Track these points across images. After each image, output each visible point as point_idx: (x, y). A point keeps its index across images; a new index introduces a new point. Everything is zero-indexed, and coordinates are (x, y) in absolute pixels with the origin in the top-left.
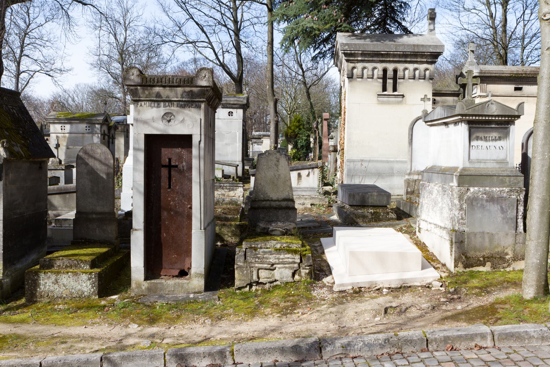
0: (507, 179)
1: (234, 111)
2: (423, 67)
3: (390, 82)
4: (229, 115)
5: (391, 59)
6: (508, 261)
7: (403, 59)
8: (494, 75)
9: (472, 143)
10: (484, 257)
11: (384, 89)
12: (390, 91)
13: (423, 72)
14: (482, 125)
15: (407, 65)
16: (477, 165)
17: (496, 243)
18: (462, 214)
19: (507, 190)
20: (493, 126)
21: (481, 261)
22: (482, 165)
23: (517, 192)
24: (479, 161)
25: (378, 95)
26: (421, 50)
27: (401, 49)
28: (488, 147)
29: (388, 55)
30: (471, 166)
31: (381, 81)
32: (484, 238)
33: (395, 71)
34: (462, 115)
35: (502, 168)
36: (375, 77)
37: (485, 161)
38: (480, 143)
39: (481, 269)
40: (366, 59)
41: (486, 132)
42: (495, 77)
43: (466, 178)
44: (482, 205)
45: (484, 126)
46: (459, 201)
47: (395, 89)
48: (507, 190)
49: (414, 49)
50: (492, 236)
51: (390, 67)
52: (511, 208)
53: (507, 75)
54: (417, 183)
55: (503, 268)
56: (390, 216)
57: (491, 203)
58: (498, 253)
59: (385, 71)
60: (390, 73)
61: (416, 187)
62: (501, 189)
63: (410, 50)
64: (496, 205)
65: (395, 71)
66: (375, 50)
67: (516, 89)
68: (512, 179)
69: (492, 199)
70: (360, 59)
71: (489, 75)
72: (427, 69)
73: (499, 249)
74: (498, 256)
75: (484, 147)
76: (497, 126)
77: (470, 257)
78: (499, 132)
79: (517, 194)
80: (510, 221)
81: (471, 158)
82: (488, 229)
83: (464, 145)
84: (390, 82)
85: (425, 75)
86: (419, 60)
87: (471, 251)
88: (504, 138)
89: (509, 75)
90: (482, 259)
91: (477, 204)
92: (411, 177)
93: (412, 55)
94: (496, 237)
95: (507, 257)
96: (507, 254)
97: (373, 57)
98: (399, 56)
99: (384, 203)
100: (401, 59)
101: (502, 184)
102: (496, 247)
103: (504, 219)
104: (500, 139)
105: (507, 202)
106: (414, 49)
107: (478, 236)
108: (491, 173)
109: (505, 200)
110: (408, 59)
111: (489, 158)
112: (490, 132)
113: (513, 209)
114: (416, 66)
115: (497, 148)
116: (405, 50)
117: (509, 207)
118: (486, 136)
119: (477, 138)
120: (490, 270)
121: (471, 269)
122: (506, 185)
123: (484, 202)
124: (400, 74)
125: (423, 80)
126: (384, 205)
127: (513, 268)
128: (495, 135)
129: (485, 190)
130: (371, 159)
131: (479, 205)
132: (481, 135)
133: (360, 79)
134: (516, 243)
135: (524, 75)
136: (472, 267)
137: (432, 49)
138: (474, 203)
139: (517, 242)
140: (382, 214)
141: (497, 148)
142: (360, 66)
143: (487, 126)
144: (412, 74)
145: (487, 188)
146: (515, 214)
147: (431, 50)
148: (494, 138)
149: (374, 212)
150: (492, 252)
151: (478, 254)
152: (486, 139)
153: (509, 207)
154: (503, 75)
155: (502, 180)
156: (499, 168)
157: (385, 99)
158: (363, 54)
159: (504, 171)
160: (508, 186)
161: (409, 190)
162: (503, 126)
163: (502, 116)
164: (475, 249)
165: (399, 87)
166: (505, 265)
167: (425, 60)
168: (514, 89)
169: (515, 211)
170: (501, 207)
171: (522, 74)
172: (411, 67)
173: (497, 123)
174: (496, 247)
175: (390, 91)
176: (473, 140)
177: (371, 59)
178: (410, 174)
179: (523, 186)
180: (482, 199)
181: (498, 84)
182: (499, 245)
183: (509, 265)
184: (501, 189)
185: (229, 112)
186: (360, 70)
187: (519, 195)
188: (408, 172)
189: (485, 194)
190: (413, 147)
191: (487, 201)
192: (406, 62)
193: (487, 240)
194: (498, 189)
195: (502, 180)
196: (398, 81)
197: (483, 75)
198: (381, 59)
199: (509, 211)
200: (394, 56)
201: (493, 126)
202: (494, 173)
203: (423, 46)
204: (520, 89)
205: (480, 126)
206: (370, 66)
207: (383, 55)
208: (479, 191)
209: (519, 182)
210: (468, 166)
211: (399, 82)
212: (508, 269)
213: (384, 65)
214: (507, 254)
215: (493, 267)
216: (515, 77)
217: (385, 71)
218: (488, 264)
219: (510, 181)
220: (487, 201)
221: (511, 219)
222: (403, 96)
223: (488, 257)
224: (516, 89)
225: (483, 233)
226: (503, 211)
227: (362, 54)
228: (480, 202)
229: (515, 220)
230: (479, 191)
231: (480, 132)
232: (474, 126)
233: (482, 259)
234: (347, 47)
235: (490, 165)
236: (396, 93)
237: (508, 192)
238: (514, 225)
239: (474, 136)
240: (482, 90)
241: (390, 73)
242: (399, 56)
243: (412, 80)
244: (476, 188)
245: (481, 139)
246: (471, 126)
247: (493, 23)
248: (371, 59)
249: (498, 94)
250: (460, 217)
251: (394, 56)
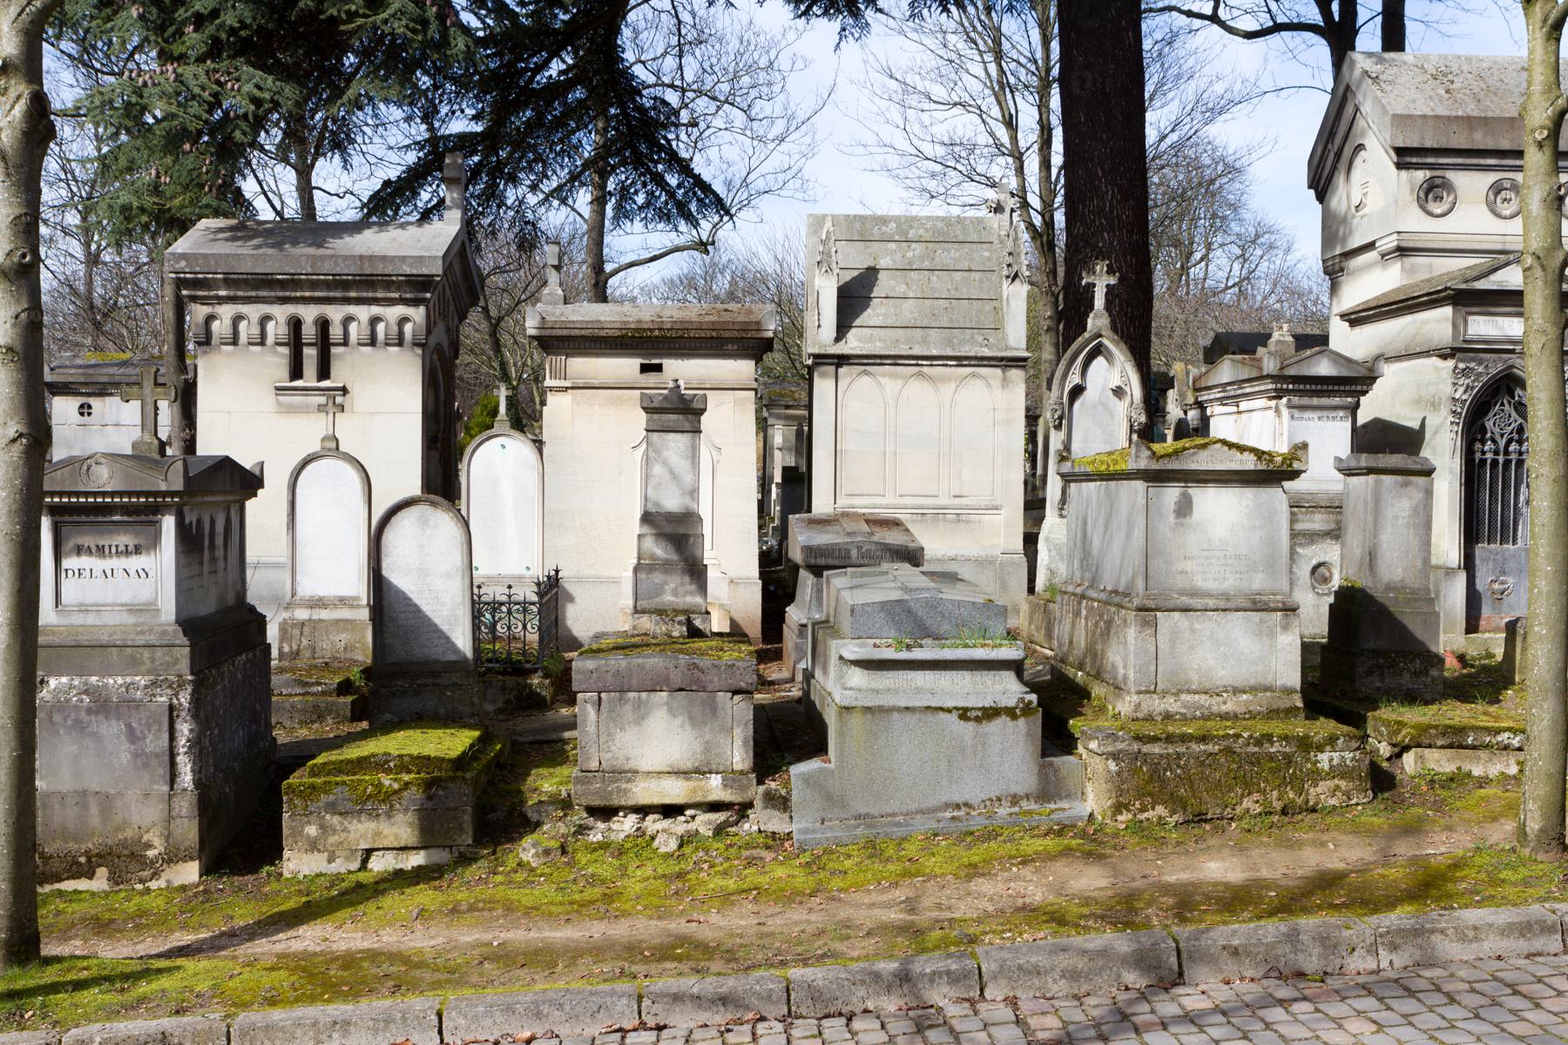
0: (146, 654)
1: (92, 401)
2: (394, 312)
3: (310, 353)
4: (82, 414)
5: (307, 294)
6: (152, 862)
7: (339, 295)
8: (577, 332)
9: (67, 563)
10: (87, 853)
11: (296, 372)
12: (310, 378)
13: (396, 328)
14: (87, 515)
15: (352, 309)
16: (77, 620)
17: (119, 819)
19: (142, 681)
20: (117, 518)
21: (81, 864)
22: (91, 619)
23: (170, 687)
24: (83, 608)
25: (277, 389)
26: (380, 269)
27: (327, 267)
28: (109, 573)
29: (293, 283)
30: (63, 621)
31: (285, 350)
32: (85, 807)
33: (323, 325)
35: (143, 624)
36: (270, 340)
37: (98, 608)
38: (85, 562)
39: (82, 884)
40: (241, 293)
41: (101, 533)
42: (583, 337)
44: (77, 722)
45: (92, 518)
47: (324, 372)
48: (142, 681)
49: (361, 267)
50: (107, 802)
51: (309, 314)
52: (155, 728)
53: (611, 333)
54: (306, 629)
55: (141, 881)
57: (101, 717)
58: (124, 844)
59: (296, 324)
60: (309, 331)
61: (305, 642)
62: (129, 679)
63: (352, 270)
64: (114, 722)
65: (323, 325)
66: (258, 271)
67: (645, 369)
68: (159, 653)
69: (102, 705)
70: (223, 293)
71: (565, 332)
73: (129, 834)
74: (126, 852)
75: (98, 572)
76: (126, 518)
77: (51, 857)
78: (136, 534)
79: (169, 692)
80: (154, 762)
81: (65, 598)
82: (95, 781)
84: (310, 353)
86: (380, 295)
87: (54, 839)
88: (148, 549)
90: (83, 860)
91: (65, 719)
93: (360, 282)
94: (118, 804)
95: (151, 853)
96: (149, 846)
97: (257, 288)
98: (328, 285)
100: (332, 294)
101: (133, 665)
102: (119, 829)
103: (135, 755)
104: (138, 550)
105: (144, 714)
106: (361, 267)
107: (70, 801)
108: (105, 639)
109: (137, 707)
110: (353, 294)
111: (110, 601)
112: (112, 532)
113: (160, 730)
114: (376, 310)
115: (133, 573)
116: (338, 270)
117: (149, 726)
118: (101, 543)
119: (79, 550)
120: (107, 888)
121: (57, 886)
122: (143, 668)
123: (83, 714)
124: (336, 332)
125: (396, 349)
127: (168, 881)
128: (124, 540)
129: (86, 684)
130: (262, 560)
131: (70, 722)
132: (88, 540)
133: (230, 348)
134: (170, 818)
135: (657, 333)
136: (60, 880)
137: (411, 266)
138: (57, 718)
139: (174, 814)
141: (133, 573)
142: (226, 312)
143: (101, 519)
144: (366, 331)
145: (94, 679)
146: (166, 744)
147: (408, 270)
148: (122, 548)
150: (109, 842)
151: (72, 846)
152: (101, 551)
153: (149, 726)
154: (603, 333)
155: (133, 657)
156: (136, 625)
157: (297, 399)
158: (229, 282)
159: (142, 633)
160: (149, 673)
161: (286, 649)
162: (143, 518)
163: (130, 494)
164: (65, 835)
165: (337, 368)
166: (147, 873)
167: (396, 295)
168: (638, 368)
169: (166, 736)
170: (129, 726)
172: (363, 313)
173: (126, 510)
174: (119, 829)
175: (310, 378)
176: (68, 555)
177: (253, 294)
178: (288, 607)
179: (187, 671)
180: (76, 707)
181: (597, 355)
182: (125, 824)
183: (156, 875)
184: (129, 679)
185: (82, 406)
186: (227, 322)
187: (176, 695)
189: (86, 692)
191: (89, 711)
192: (347, 301)
193: (94, 811)
194: (120, 680)
195: (133, 657)
196: (334, 350)
197: (548, 333)
198: (281, 294)
199: (151, 736)
200: (314, 285)
201: (117, 518)
202: (117, 638)
203: (384, 258)
204: (658, 368)
205: (83, 518)
206: (253, 311)
207: (282, 284)
208: (71, 687)
209: (177, 661)
210: (55, 622)
211: (338, 355)
212: (153, 885)
213: (291, 309)
214: (149, 846)
215: (115, 879)
217: (296, 324)
218: (102, 872)
219: (153, 660)
220: (89, 711)
221: (157, 756)
222: (344, 390)
223: (99, 855)
224: (645, 369)
225: (84, 792)
226: (132, 736)
227: (225, 280)
228: (73, 716)
229: (167, 758)
230: (71, 687)
231: (86, 533)
232: (67, 518)
233: (83, 860)
234: (183, 263)
235: (112, 619)
236: (325, 384)
237: (146, 687)
238: (163, 771)
239: (69, 545)
241: (309, 331)
242: (328, 285)
243: (369, 349)
244: (64, 680)
245: (89, 552)
246: (58, 518)
247: (1014, 139)
248: (253, 294)
249: (596, 382)
251: (314, 285)
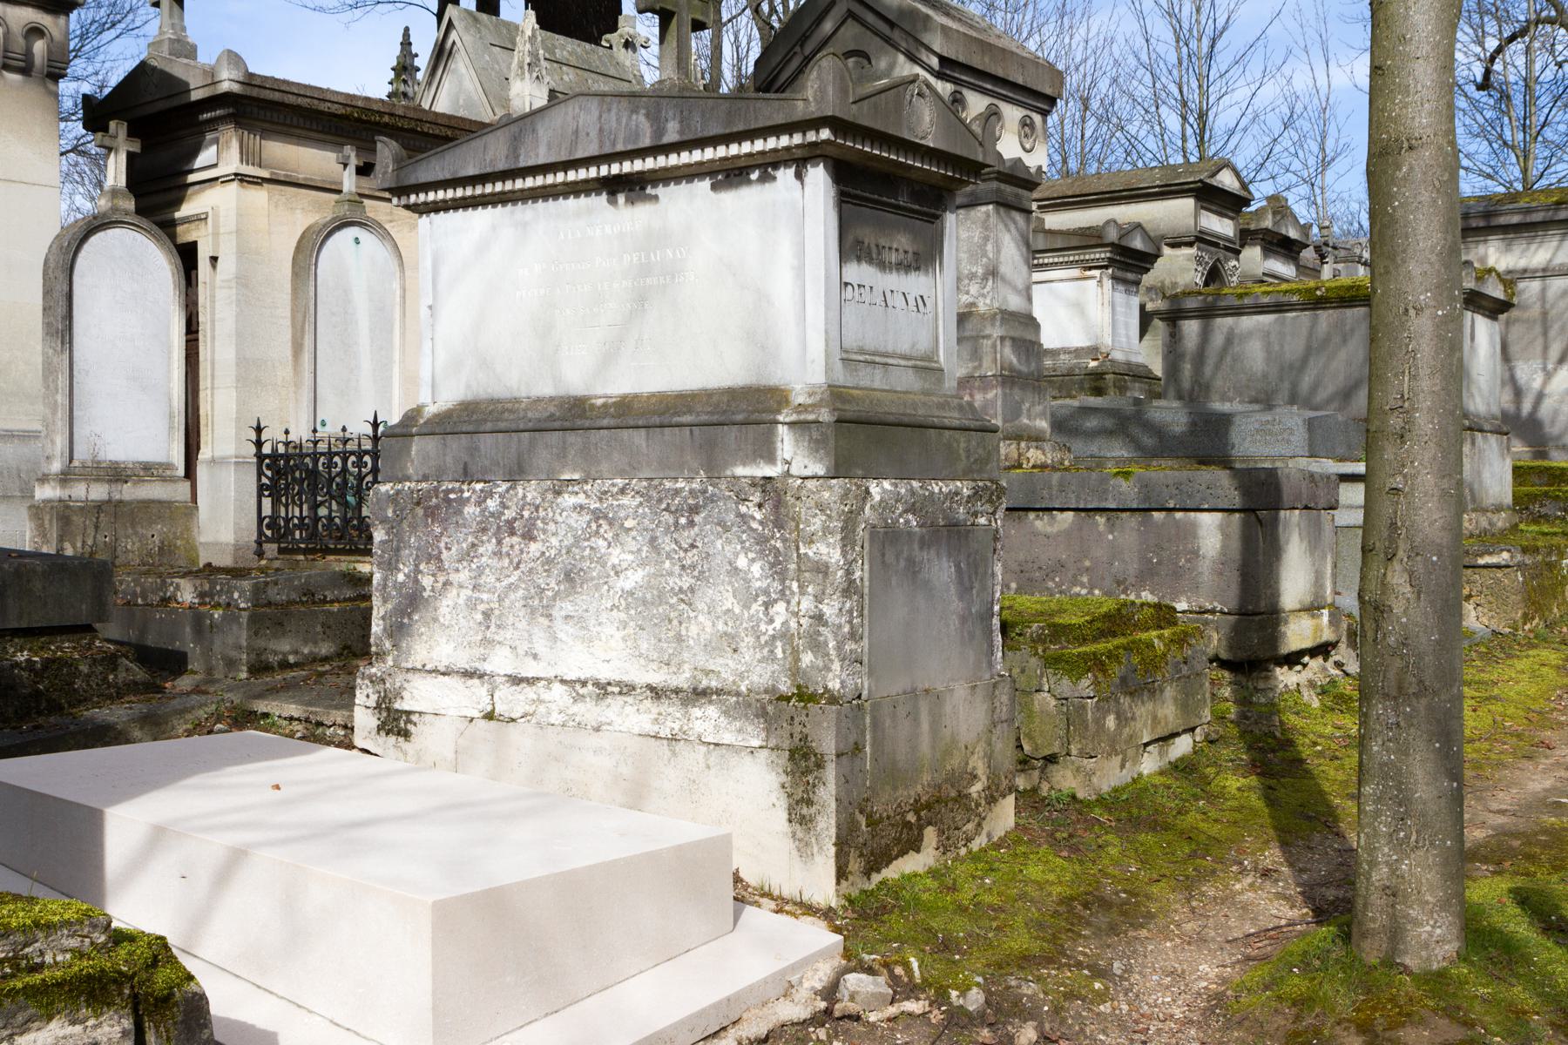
8: (291, 99)
18: (850, 612)
34: (839, 125)
42: (296, 109)
43: (863, 431)
46: (844, 554)
53: (334, 108)
56: (122, 675)
71: (276, 96)
72: (35, 31)
83: (827, 278)
85: (28, 54)
89: (341, 111)
92: (79, 491)
99: (82, 612)
126: (83, 620)
135: (386, 119)
140: (84, 668)
149: (47, 663)
154: (324, 107)
171: (381, 114)
188: (56, 466)
190: (76, 354)
216: (359, 120)
240: (246, 156)
249: (301, 177)
250: (846, 629)
